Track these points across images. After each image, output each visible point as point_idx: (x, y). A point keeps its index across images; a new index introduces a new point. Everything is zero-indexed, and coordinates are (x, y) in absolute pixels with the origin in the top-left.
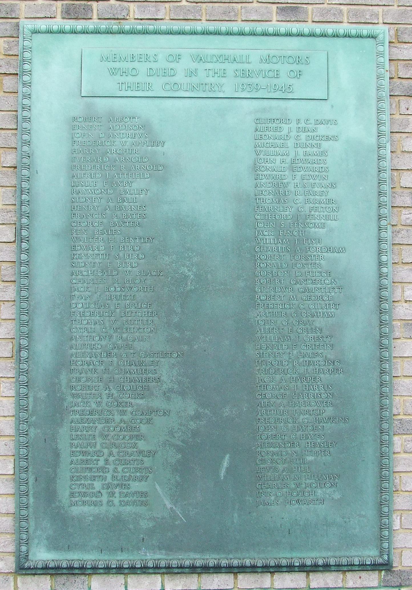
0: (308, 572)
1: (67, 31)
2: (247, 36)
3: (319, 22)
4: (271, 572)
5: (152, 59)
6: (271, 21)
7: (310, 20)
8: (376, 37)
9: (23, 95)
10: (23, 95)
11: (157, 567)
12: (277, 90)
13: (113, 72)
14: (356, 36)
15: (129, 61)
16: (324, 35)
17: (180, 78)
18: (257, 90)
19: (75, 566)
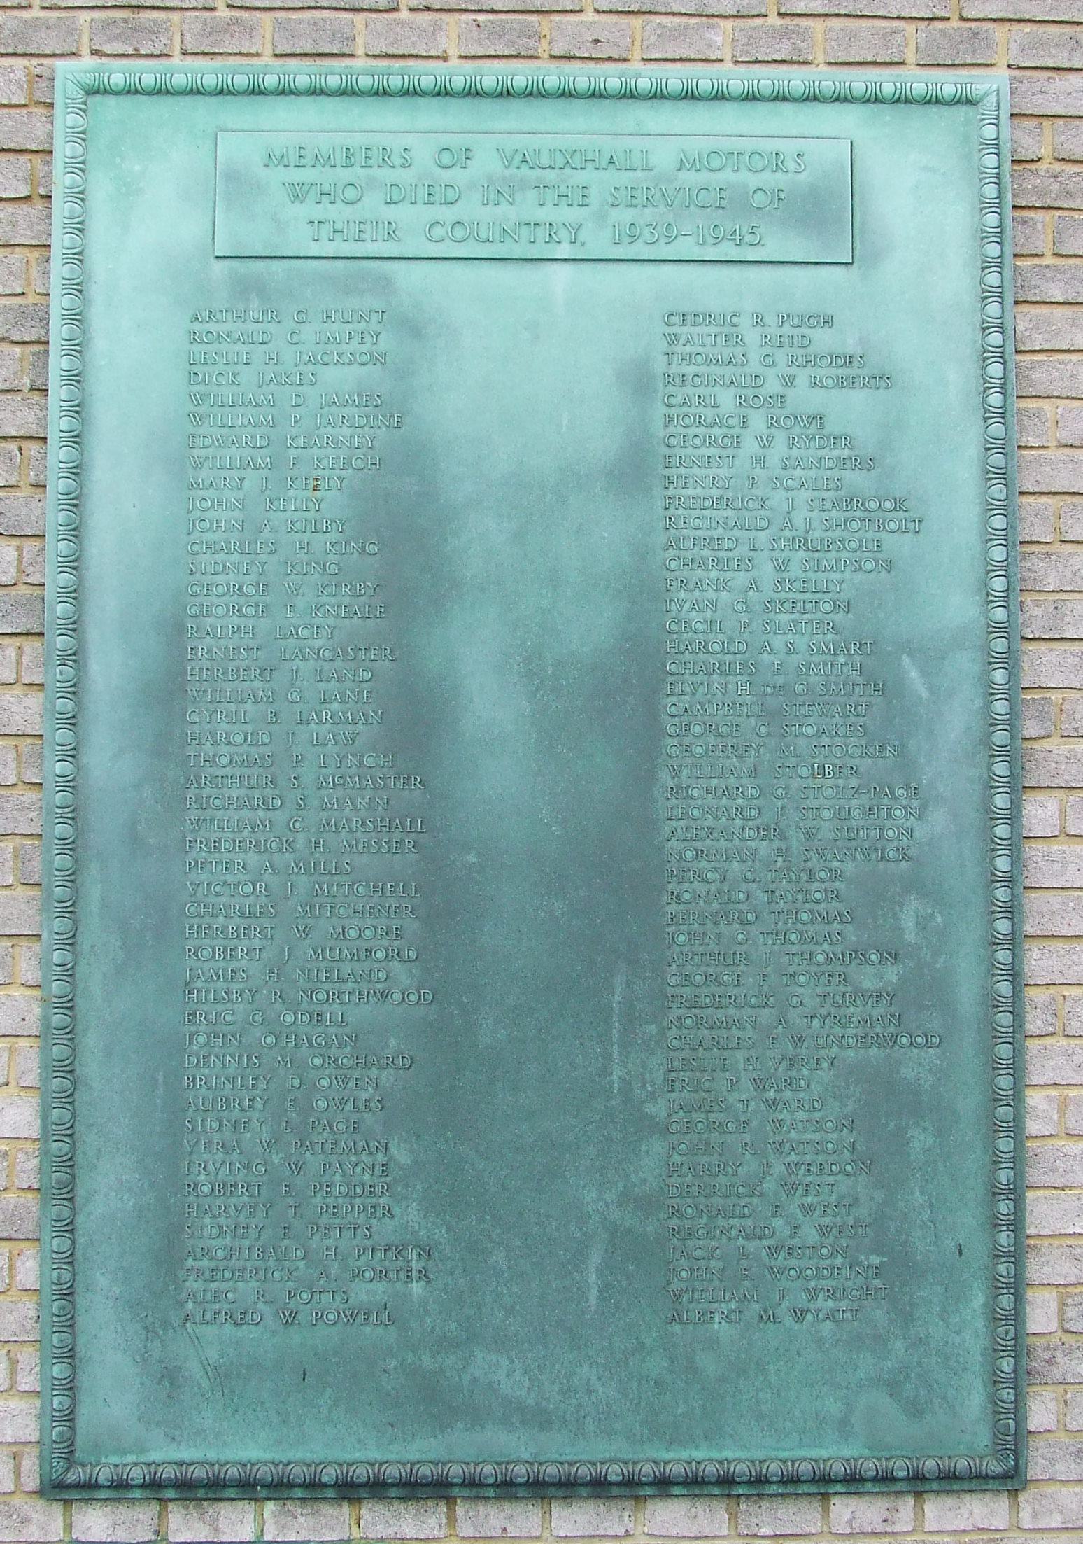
0: (355, 1501)
1: (241, 90)
2: (797, 104)
3: (836, 63)
4: (65, 1501)
5: (397, 160)
6: (625, 60)
7: (85, 51)
8: (978, 103)
9: (64, 254)
10: (64, 254)
11: (697, 1482)
12: (723, 239)
13: (297, 194)
14: (278, 92)
15: (292, 164)
16: (568, 94)
17: (470, 209)
18: (671, 240)
19: (325, 1479)
